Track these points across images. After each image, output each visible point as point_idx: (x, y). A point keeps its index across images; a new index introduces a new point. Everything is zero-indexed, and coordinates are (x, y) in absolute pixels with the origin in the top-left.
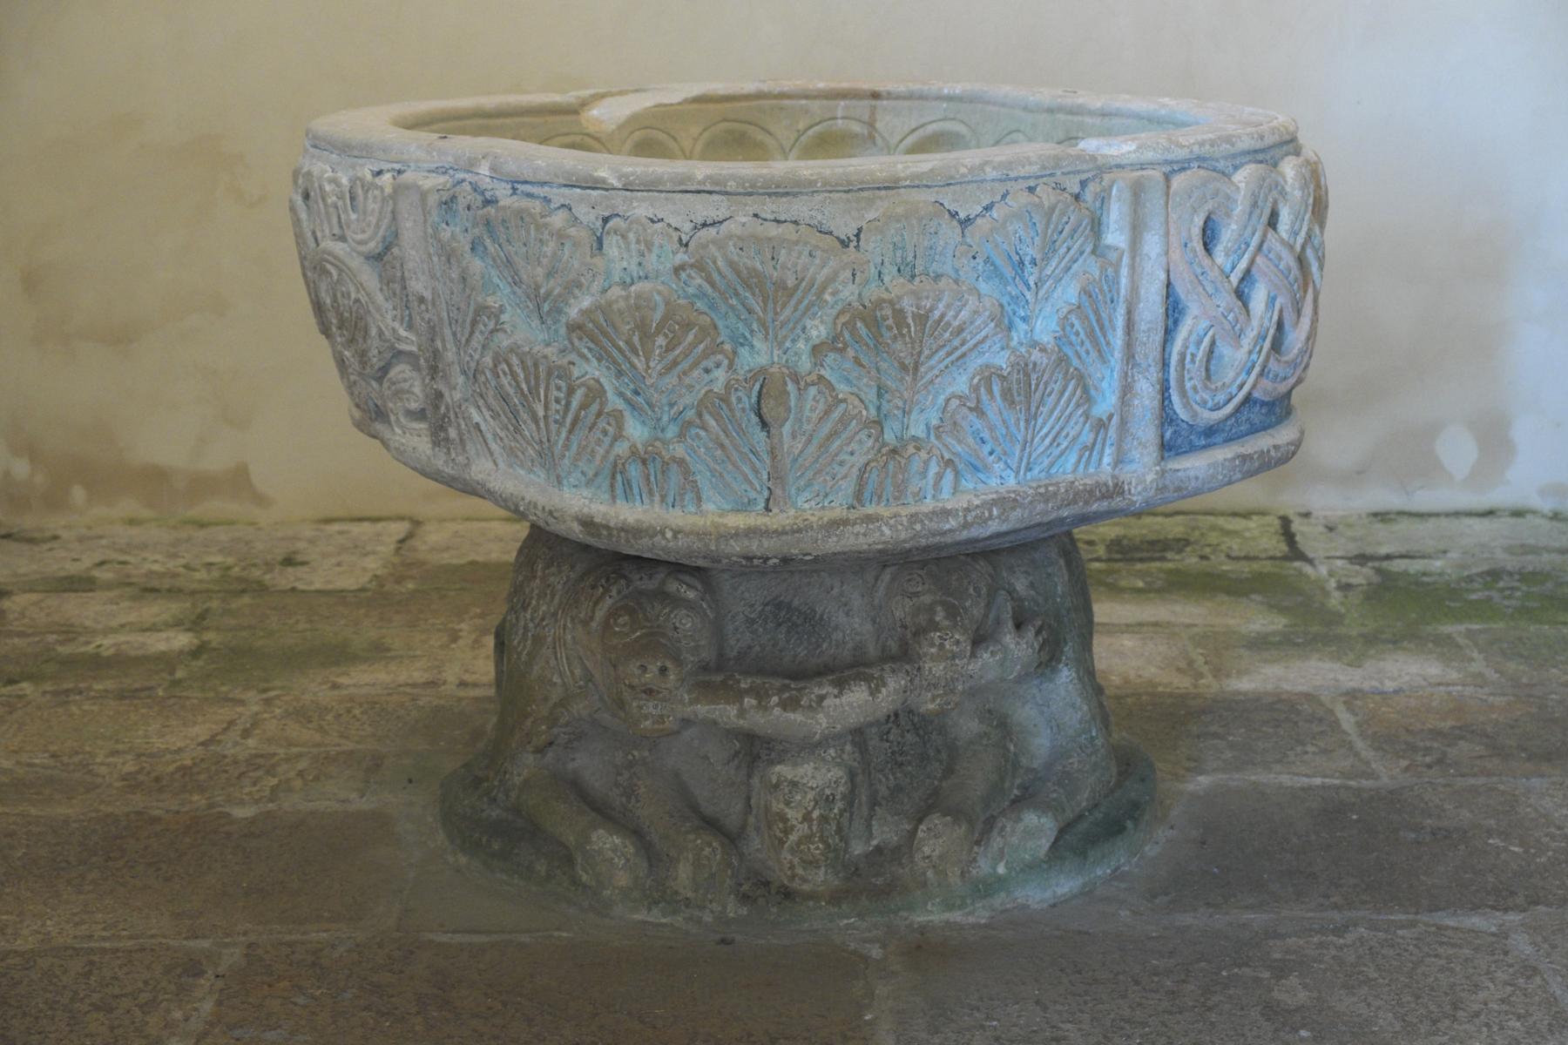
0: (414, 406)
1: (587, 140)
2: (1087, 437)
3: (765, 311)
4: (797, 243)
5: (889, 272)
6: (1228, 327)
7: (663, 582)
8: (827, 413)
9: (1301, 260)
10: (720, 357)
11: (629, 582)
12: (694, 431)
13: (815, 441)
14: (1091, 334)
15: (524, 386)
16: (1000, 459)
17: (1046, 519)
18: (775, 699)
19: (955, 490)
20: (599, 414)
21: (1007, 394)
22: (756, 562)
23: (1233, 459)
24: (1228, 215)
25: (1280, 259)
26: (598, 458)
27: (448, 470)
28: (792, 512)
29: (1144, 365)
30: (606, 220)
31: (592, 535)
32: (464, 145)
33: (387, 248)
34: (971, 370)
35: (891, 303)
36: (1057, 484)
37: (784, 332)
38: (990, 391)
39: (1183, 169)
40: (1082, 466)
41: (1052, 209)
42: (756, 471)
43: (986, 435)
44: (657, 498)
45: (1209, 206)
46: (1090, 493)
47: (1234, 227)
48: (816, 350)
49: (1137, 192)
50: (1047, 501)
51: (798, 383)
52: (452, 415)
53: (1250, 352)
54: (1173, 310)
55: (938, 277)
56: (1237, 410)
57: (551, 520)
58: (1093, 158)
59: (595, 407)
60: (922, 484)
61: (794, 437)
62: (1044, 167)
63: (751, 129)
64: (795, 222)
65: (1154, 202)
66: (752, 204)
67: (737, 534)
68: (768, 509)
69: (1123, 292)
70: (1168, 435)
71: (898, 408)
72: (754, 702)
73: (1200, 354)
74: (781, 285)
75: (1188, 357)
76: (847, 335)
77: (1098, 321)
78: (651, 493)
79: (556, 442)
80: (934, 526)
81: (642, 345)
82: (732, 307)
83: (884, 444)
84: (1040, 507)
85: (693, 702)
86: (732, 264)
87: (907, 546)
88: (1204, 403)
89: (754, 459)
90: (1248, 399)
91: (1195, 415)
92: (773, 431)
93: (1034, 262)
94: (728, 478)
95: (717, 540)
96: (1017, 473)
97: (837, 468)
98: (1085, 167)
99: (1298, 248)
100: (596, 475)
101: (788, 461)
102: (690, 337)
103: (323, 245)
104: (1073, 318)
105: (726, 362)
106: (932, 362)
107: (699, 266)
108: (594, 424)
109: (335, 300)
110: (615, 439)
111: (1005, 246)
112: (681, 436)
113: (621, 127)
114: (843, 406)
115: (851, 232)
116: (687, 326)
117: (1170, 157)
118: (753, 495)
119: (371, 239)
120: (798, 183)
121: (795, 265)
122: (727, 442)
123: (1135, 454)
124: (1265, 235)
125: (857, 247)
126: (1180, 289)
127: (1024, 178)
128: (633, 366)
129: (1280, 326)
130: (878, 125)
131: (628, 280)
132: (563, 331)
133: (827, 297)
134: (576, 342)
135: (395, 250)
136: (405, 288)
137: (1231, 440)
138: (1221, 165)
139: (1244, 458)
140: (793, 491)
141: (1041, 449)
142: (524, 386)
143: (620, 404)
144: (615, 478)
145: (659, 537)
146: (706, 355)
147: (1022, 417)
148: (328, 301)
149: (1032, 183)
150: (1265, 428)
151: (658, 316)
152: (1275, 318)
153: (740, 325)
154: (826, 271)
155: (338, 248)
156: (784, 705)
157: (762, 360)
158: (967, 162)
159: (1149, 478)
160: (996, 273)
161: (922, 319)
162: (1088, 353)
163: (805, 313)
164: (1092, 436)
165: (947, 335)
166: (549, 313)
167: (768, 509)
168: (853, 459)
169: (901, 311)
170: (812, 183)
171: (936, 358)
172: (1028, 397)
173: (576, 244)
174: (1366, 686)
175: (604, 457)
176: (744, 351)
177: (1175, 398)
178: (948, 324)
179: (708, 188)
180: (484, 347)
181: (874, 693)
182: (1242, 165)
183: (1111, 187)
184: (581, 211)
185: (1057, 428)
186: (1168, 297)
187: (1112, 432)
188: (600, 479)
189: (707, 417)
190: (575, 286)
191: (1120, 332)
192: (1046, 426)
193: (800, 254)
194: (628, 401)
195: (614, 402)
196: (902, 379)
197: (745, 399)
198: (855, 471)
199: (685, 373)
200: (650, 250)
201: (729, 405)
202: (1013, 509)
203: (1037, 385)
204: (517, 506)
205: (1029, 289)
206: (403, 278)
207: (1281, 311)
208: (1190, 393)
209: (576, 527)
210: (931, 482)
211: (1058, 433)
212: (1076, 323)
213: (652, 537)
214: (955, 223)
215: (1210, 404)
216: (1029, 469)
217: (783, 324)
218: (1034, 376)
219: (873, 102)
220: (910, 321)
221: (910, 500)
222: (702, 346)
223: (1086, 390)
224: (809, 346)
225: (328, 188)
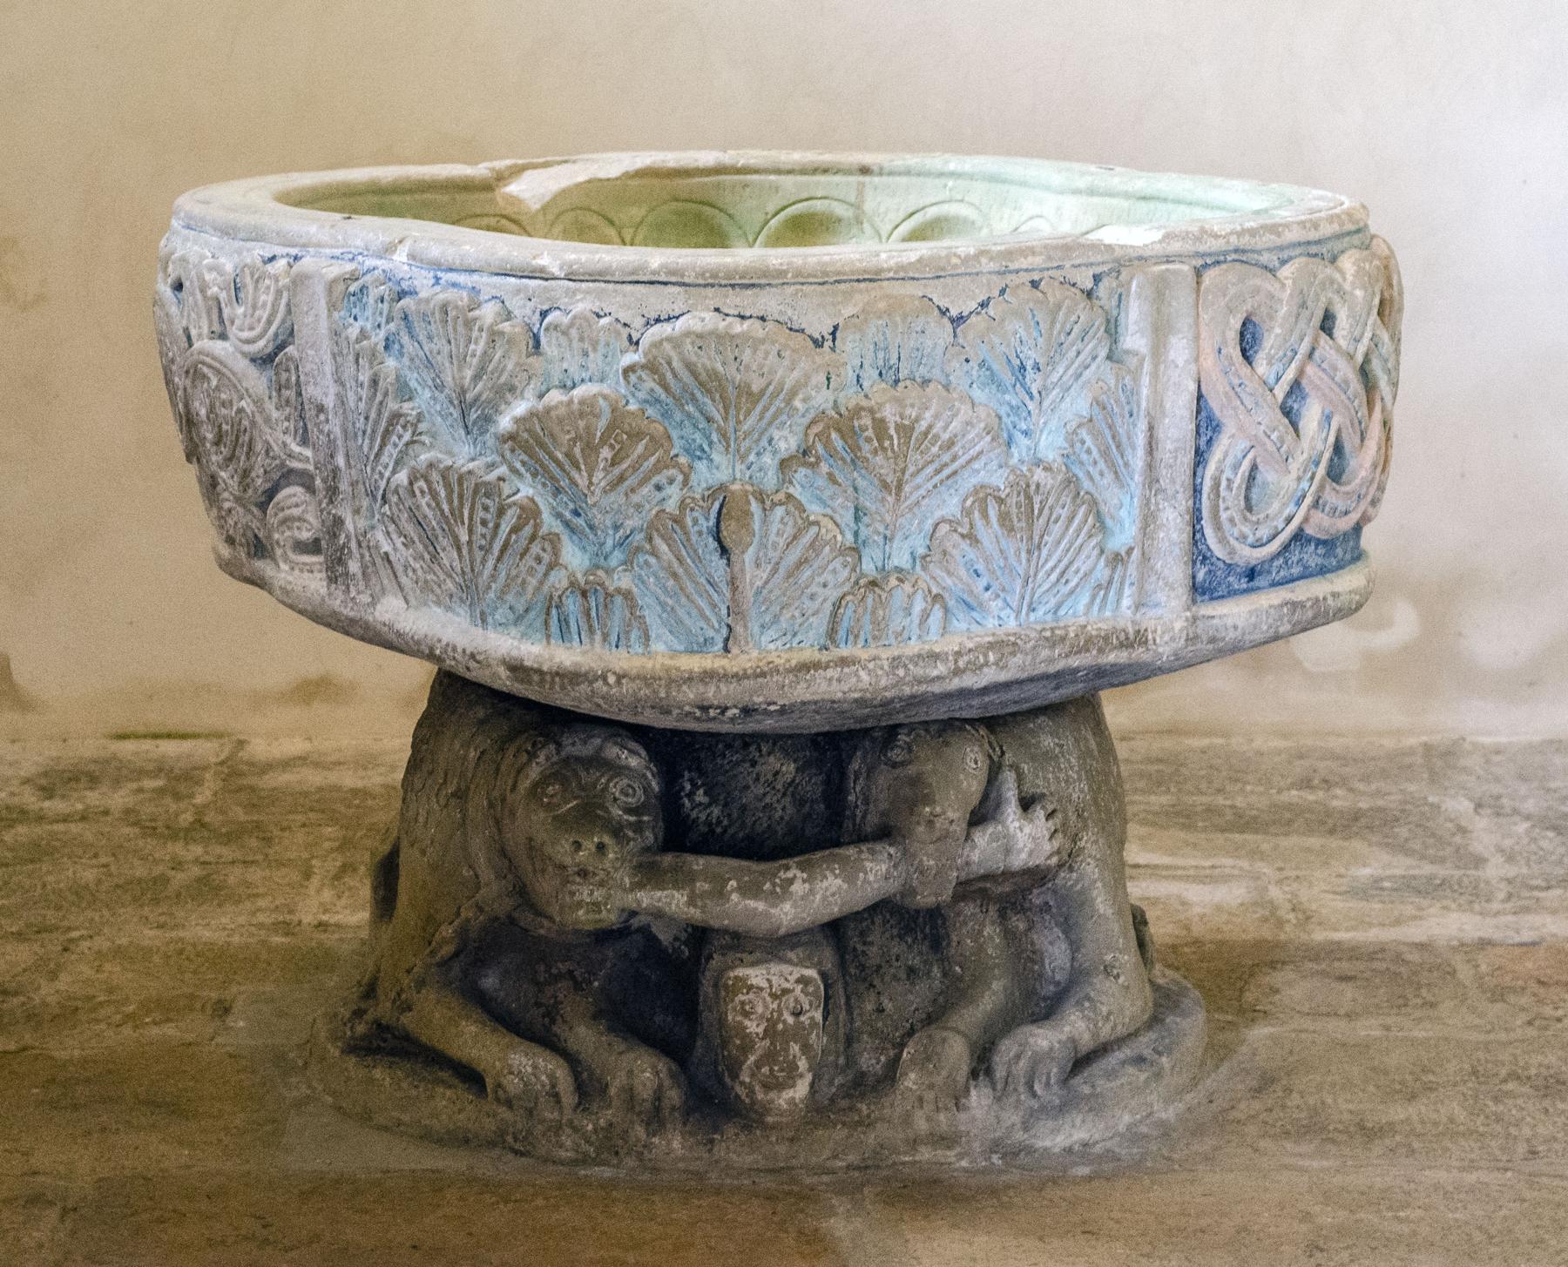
0: (305, 535)
1: (504, 222)
2: (1102, 572)
3: (725, 419)
4: (762, 341)
5: (870, 375)
6: (1271, 447)
7: (601, 748)
9: (1364, 372)
10: (672, 472)
11: (559, 745)
12: (641, 558)
13: (782, 571)
14: (1105, 453)
15: (445, 507)
16: (998, 596)
17: (1052, 669)
18: (733, 883)
19: (945, 631)
20: (533, 538)
21: (1004, 518)
22: (712, 713)
23: (1281, 606)
24: (1271, 318)
25: (1335, 369)
26: (530, 589)
27: (347, 612)
28: (755, 654)
30: (544, 314)
31: (522, 681)
32: (369, 230)
33: (281, 347)
35: (871, 411)
36: (1066, 627)
37: (747, 443)
38: (985, 515)
40: (1096, 608)
41: (1059, 307)
42: (714, 606)
43: (980, 567)
44: (598, 637)
45: (1248, 307)
46: (1105, 641)
47: (1278, 330)
48: (784, 464)
49: (1160, 291)
50: (1053, 646)
51: (763, 502)
52: (353, 545)
53: (1299, 479)
54: (1206, 425)
55: (926, 382)
56: (1286, 548)
57: (472, 664)
58: (1109, 248)
59: (527, 531)
60: (906, 622)
61: (758, 566)
62: (1050, 258)
63: (708, 210)
64: (763, 319)
65: (1181, 300)
66: (713, 297)
67: (690, 679)
68: (726, 650)
69: (1144, 404)
70: (1201, 576)
71: (879, 533)
73: (1239, 480)
74: (744, 390)
75: (1224, 484)
77: (1114, 437)
78: (591, 631)
79: (481, 573)
80: (918, 671)
81: (585, 457)
82: (689, 415)
83: (862, 575)
84: (1045, 653)
85: (640, 886)
86: (690, 367)
87: (888, 694)
88: (1242, 538)
89: (711, 591)
90: (1299, 537)
91: (1232, 552)
92: (733, 558)
94: (681, 612)
95: (668, 686)
96: (1018, 613)
97: (808, 603)
98: (1099, 258)
99: (1360, 358)
100: (527, 611)
101: (750, 594)
102: (640, 448)
103: (197, 345)
104: (1083, 433)
105: (680, 478)
106: (919, 479)
107: (651, 367)
108: (527, 550)
109: (212, 409)
110: (551, 567)
111: (1003, 348)
112: (628, 563)
113: (545, 209)
114: (814, 529)
115: (826, 330)
116: (636, 436)
117: (1202, 248)
118: (711, 633)
119: (260, 337)
120: (765, 273)
121: (761, 366)
122: (680, 571)
123: (1161, 597)
124: (1316, 340)
125: (833, 349)
126: (1214, 403)
127: (1026, 270)
128: (574, 483)
129: (1338, 449)
130: (869, 206)
131: (569, 383)
132: (491, 442)
134: (508, 454)
135: (290, 349)
136: (299, 394)
138: (1265, 258)
139: (1295, 605)
140: (756, 629)
141: (1046, 586)
142: (445, 507)
143: (557, 527)
144: (550, 616)
145: (600, 682)
146: (657, 469)
147: (1024, 547)
148: (203, 412)
150: (1322, 571)
151: (602, 424)
152: (1332, 439)
153: (698, 436)
154: (796, 374)
155: (219, 347)
156: (744, 891)
157: (722, 476)
158: (962, 251)
159: (1178, 625)
160: (993, 378)
161: (906, 431)
162: (1102, 474)
163: (770, 424)
164: (1107, 572)
165: (935, 450)
166: (475, 423)
167: (726, 650)
168: (827, 592)
169: (882, 421)
170: (781, 273)
171: (923, 475)
172: (1030, 526)
173: (511, 342)
174: (1497, 936)
175: (538, 589)
176: (701, 466)
177: (1206, 524)
178: (936, 437)
179: (663, 278)
180: (397, 463)
181: (850, 880)
182: (1291, 258)
183: (1129, 283)
184: (514, 304)
186: (1198, 412)
187: (1132, 569)
188: (532, 614)
189: (658, 541)
190: (508, 390)
192: (1051, 557)
193: (767, 353)
194: (567, 524)
195: (549, 523)
196: (883, 500)
197: (702, 521)
198: (828, 607)
199: (633, 490)
200: (595, 350)
201: (683, 527)
202: (1013, 654)
203: (1041, 511)
204: (432, 649)
205: (1032, 398)
206: (298, 383)
207: (1339, 431)
208: (1226, 525)
209: (503, 672)
210: (917, 622)
212: (1089, 442)
213: (591, 683)
214: (946, 320)
215: (1251, 539)
217: (746, 435)
218: (1037, 499)
219: (861, 178)
220: (892, 432)
221: (893, 641)
222: (653, 460)
223: (1098, 515)
224: (776, 461)
225: (208, 277)
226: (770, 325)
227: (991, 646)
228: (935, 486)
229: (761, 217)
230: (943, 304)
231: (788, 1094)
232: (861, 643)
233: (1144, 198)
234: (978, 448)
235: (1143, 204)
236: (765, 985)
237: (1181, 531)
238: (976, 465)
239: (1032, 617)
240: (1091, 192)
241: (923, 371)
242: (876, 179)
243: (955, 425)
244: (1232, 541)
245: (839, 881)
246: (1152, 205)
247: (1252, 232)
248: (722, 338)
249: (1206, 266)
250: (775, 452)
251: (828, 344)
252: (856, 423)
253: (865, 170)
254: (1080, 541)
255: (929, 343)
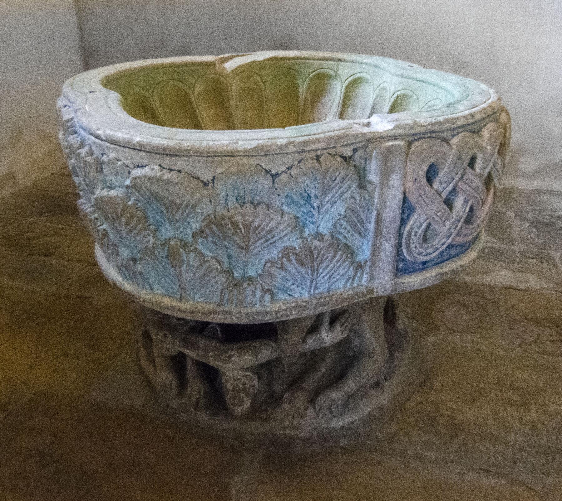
2: (351, 273)
4: (177, 183)
5: (232, 200)
8: (201, 265)
14: (354, 227)
18: (211, 354)
21: (299, 261)
25: (472, 182)
29: (388, 237)
34: (279, 249)
35: (230, 218)
36: (331, 296)
39: (420, 139)
41: (327, 170)
45: (432, 160)
47: (446, 169)
48: (194, 235)
50: (324, 305)
54: (407, 209)
62: (328, 144)
64: (180, 171)
65: (398, 160)
69: (375, 205)
72: (203, 353)
74: (173, 202)
75: (413, 233)
76: (207, 231)
93: (316, 197)
98: (358, 140)
113: (232, 72)
114: (207, 264)
115: (209, 177)
117: (413, 132)
125: (213, 187)
126: (412, 201)
129: (471, 209)
130: (339, 72)
133: (198, 210)
137: (437, 264)
138: (444, 135)
149: (319, 153)
151: (120, 209)
162: (352, 235)
165: (263, 233)
170: (188, 151)
171: (258, 244)
177: (405, 251)
179: (138, 148)
182: (458, 134)
183: (372, 151)
185: (332, 271)
191: (373, 224)
193: (180, 189)
205: (314, 209)
210: (258, 299)
211: (335, 272)
216: (316, 288)
220: (241, 226)
226: (181, 176)
227: (294, 308)
228: (265, 247)
229: (307, 73)
230: (268, 168)
231: (240, 408)
232: (233, 306)
233: (418, 81)
234: (285, 232)
235: (418, 83)
236: (231, 375)
237: (391, 253)
238: (285, 239)
239: (317, 291)
240: (402, 76)
241: (257, 198)
242: (343, 63)
243: (272, 224)
244: (415, 255)
245: (250, 357)
246: (422, 83)
247: (440, 123)
248: (159, 180)
249: (415, 140)
250: (191, 228)
251: (211, 185)
252: (223, 222)
253: (340, 60)
254: (339, 264)
255: (260, 186)
